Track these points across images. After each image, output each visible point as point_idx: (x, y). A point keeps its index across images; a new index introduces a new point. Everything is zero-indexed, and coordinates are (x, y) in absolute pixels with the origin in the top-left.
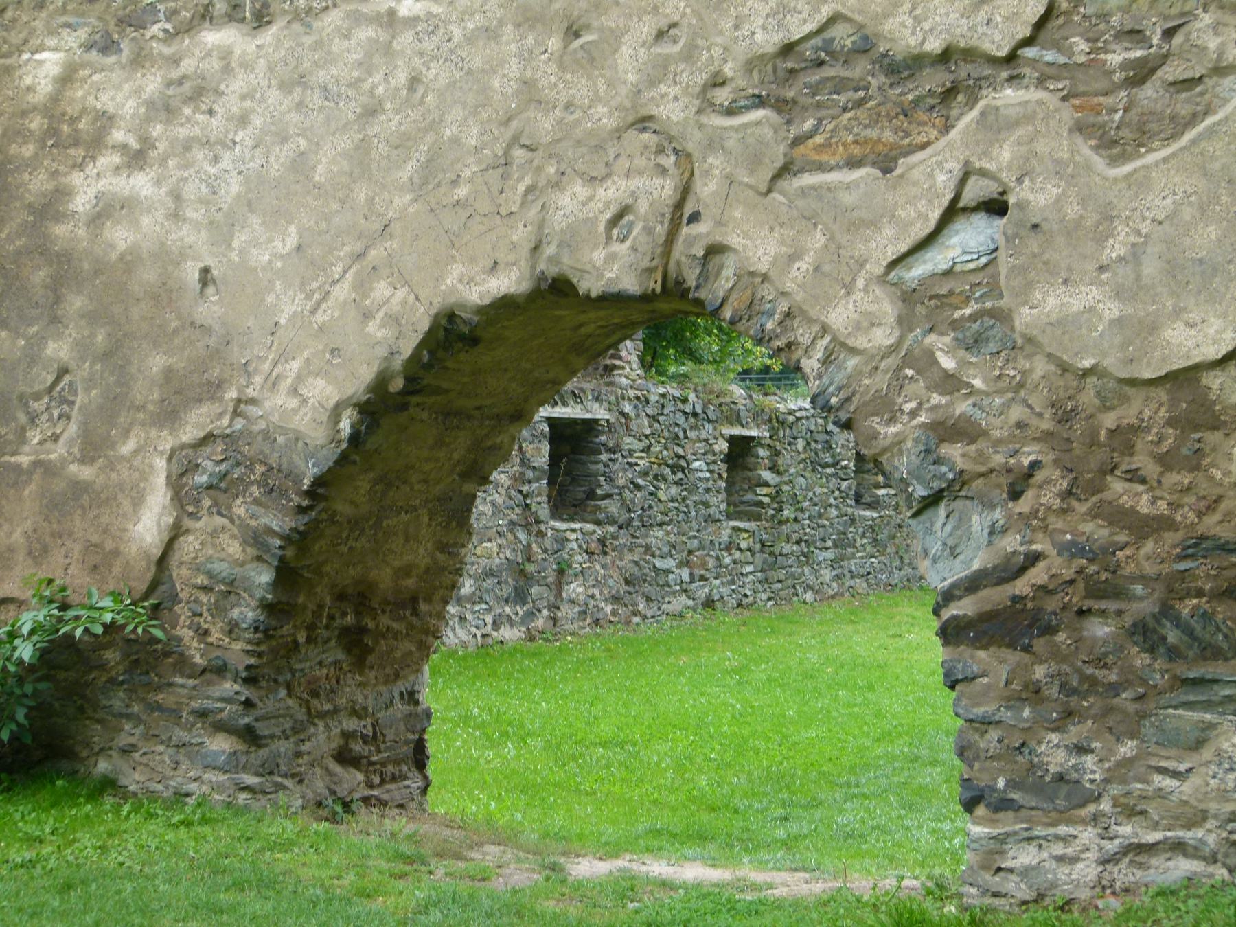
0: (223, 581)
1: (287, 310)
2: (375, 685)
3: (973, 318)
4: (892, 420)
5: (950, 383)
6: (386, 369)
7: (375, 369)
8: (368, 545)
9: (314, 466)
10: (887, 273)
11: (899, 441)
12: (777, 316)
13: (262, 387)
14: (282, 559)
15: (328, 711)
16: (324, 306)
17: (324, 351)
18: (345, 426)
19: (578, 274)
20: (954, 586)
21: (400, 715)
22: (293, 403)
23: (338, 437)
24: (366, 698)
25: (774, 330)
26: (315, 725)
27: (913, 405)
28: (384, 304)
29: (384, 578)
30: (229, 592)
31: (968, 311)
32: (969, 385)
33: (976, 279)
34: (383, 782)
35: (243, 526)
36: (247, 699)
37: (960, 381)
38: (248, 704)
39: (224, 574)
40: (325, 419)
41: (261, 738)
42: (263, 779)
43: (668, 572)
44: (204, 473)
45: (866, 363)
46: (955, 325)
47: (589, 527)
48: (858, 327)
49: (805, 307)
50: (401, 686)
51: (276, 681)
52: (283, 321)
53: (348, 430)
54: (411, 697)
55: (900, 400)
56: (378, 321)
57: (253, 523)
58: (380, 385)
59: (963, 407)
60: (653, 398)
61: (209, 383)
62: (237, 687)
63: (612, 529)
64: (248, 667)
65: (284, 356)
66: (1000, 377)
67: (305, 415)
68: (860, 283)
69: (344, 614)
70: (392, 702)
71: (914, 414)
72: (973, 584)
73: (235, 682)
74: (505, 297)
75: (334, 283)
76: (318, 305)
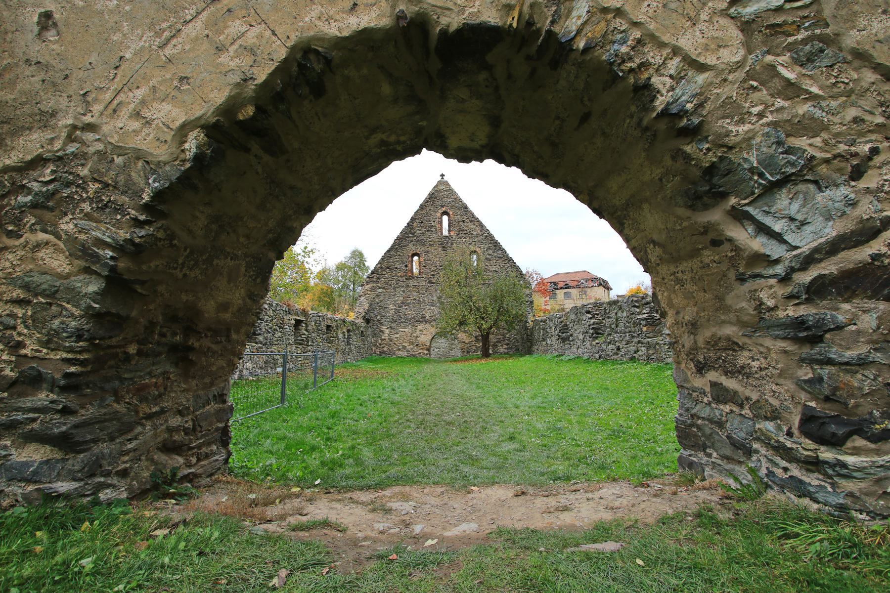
0: (43, 294)
1: (133, 46)
2: (195, 391)
3: (805, 42)
4: (741, 121)
5: (792, 90)
6: (239, 94)
7: (226, 94)
8: (200, 277)
9: (154, 181)
10: (728, 8)
11: (748, 139)
12: (629, 43)
13: (102, 114)
14: (113, 269)
15: (156, 412)
16: (174, 41)
17: (171, 79)
18: (191, 146)
19: (439, 11)
20: (816, 250)
21: (212, 412)
22: (136, 125)
23: (182, 156)
24: (188, 400)
25: (628, 53)
26: (143, 425)
27: (760, 108)
28: (239, 38)
29: (209, 308)
30: (50, 304)
31: (800, 37)
32: (807, 92)
33: (806, 13)
34: (199, 460)
35: (71, 240)
36: (65, 407)
37: (800, 88)
38: (66, 411)
39: (44, 286)
40: (169, 138)
41: (79, 443)
42: (82, 483)
43: (278, 360)
44: (28, 194)
45: (716, 77)
46: (790, 48)
47: (254, 344)
48: (706, 48)
49: (657, 34)
50: (214, 390)
51: (102, 389)
52: (128, 56)
53: (194, 150)
54: (221, 398)
55: (747, 105)
56: (232, 53)
57: (83, 237)
58: (229, 109)
59: (804, 108)
60: (274, 305)
61: (42, 112)
62: (53, 396)
63: (260, 345)
64: (67, 375)
65: (128, 86)
66: (834, 84)
67: (148, 135)
68: (704, 16)
69: (175, 334)
70: (208, 401)
71: (761, 115)
72: (834, 247)
73: (52, 391)
74: (365, 30)
75: (186, 22)
76: (168, 41)
